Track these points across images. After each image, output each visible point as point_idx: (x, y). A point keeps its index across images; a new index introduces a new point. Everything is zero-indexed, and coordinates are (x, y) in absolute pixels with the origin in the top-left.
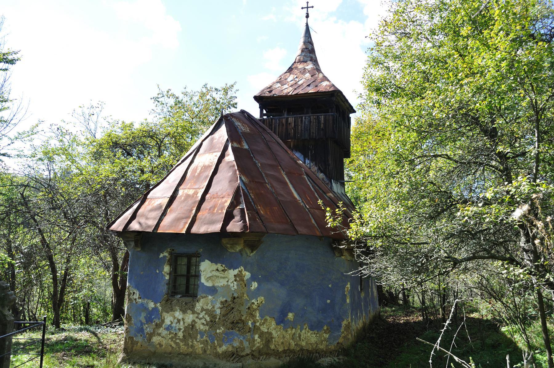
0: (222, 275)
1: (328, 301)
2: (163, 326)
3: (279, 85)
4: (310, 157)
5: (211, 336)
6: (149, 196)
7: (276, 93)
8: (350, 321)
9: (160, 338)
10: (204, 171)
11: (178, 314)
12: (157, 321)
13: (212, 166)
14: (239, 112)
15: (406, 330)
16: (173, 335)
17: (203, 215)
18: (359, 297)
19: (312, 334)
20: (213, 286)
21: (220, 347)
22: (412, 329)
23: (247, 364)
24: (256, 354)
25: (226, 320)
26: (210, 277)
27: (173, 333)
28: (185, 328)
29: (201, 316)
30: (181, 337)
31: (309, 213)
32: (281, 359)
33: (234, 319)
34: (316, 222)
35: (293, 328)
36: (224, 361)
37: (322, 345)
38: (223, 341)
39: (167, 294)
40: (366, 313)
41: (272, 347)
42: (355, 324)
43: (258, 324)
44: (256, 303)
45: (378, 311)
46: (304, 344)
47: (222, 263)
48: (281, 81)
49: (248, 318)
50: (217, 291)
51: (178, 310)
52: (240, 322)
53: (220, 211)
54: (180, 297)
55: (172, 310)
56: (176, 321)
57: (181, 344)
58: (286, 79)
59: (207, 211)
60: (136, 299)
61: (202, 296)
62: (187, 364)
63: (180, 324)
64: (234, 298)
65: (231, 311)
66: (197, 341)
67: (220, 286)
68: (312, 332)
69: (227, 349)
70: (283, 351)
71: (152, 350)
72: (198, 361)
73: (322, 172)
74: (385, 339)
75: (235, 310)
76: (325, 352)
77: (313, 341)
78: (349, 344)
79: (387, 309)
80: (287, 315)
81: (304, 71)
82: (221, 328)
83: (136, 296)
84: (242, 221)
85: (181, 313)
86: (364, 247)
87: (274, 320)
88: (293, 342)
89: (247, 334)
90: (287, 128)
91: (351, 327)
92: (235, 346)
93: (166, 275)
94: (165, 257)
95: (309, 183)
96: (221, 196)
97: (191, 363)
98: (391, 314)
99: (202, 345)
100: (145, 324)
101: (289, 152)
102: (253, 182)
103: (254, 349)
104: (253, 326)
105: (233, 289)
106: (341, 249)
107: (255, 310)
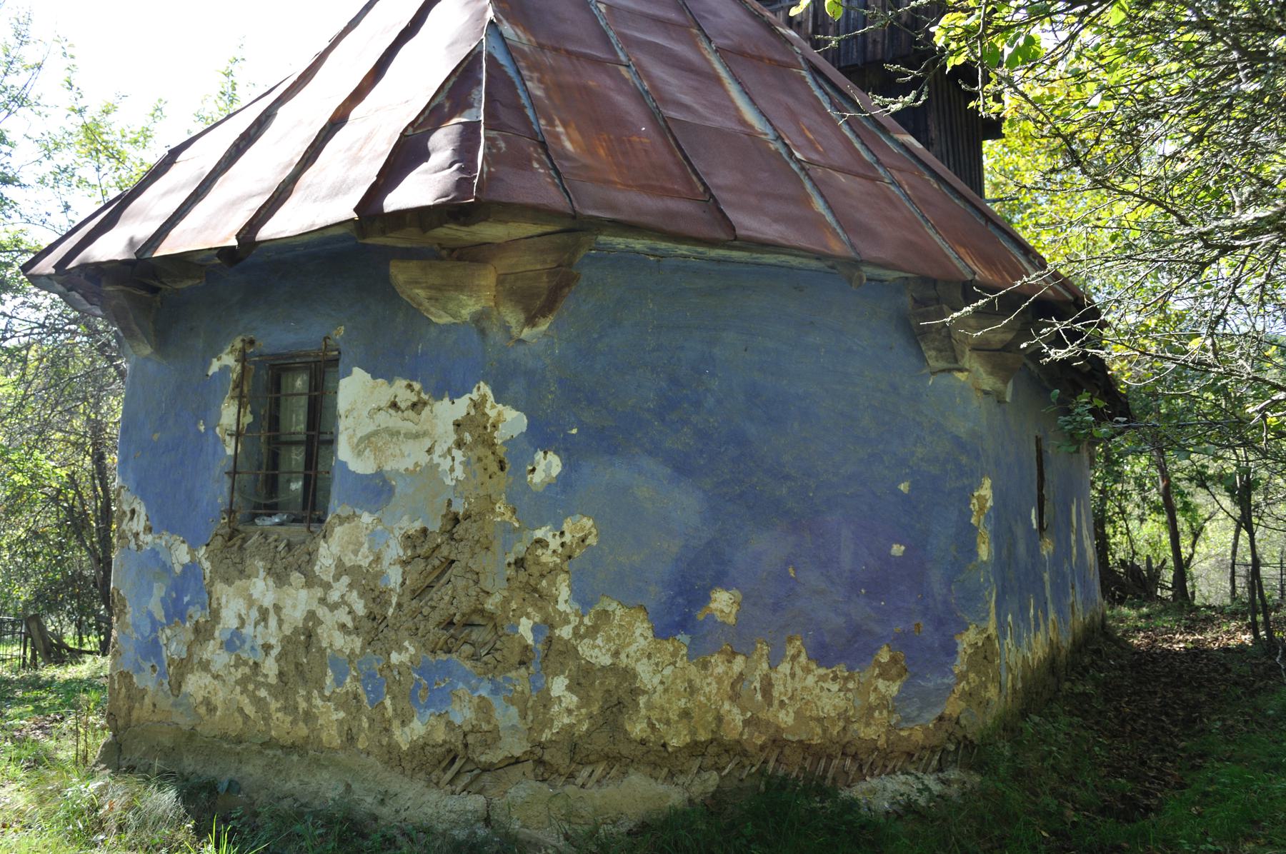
0: (409, 425)
1: (897, 550)
2: (217, 633)
8: (992, 630)
9: (207, 679)
11: (262, 588)
12: (199, 615)
15: (1201, 672)
16: (247, 670)
18: (1034, 552)
19: (822, 678)
20: (379, 474)
21: (403, 723)
22: (1221, 671)
24: (557, 758)
25: (426, 611)
26: (368, 437)
27: (245, 663)
28: (287, 640)
29: (334, 596)
30: (273, 680)
33: (452, 610)
34: (830, 207)
35: (734, 654)
36: (419, 785)
37: (868, 725)
38: (413, 696)
39: (231, 512)
40: (1059, 611)
42: (1018, 644)
44: (554, 543)
45: (1099, 611)
46: (786, 718)
50: (391, 490)
51: (262, 574)
52: (476, 619)
54: (281, 524)
55: (243, 574)
56: (254, 614)
57: (274, 705)
60: (136, 535)
61: (339, 516)
62: (289, 785)
63: (266, 627)
64: (456, 520)
65: (443, 573)
66: (323, 697)
67: (402, 470)
68: (822, 671)
69: (429, 733)
70: (687, 746)
71: (185, 722)
72: (325, 775)
74: (1128, 703)
75: (456, 569)
76: (886, 755)
78: (989, 721)
79: (1125, 610)
80: (707, 599)
82: (406, 644)
85: (270, 582)
87: (642, 615)
88: (736, 710)
89: (513, 674)
91: (999, 655)
93: (228, 438)
94: (225, 370)
97: (302, 783)
98: (1139, 624)
99: (342, 715)
103: (546, 736)
104: (542, 638)
105: (449, 482)
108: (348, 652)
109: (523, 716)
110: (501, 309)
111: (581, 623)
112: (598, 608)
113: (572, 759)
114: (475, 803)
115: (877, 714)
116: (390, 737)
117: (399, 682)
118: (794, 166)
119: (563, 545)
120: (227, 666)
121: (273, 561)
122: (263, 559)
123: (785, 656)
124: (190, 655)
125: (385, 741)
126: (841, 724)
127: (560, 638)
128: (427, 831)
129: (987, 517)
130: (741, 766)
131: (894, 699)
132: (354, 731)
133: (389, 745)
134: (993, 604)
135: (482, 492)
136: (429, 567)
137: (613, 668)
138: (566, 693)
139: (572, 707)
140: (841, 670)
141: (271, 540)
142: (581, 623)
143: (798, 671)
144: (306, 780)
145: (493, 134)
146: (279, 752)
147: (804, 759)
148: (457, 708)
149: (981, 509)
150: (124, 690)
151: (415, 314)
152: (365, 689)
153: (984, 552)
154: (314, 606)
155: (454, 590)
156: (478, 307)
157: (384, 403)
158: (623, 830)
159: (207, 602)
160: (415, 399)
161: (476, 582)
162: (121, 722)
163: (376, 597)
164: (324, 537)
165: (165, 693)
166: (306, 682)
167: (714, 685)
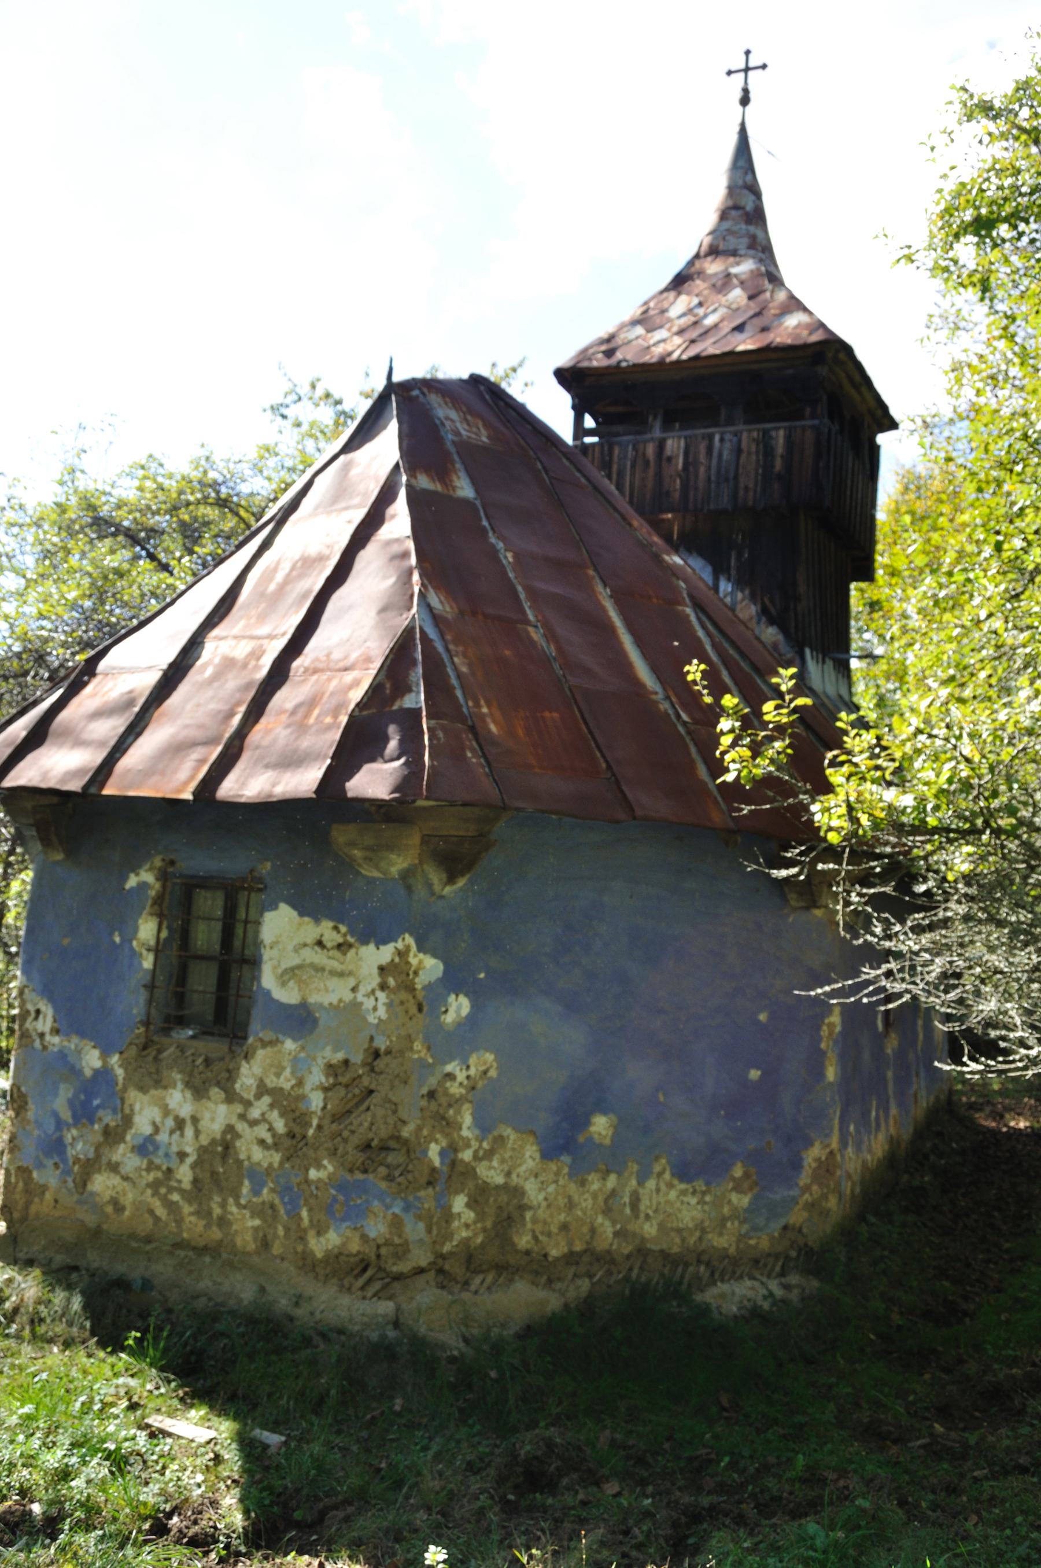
0: (335, 964)
1: (754, 1074)
2: (128, 1138)
3: (639, 330)
4: (733, 572)
5: (288, 1189)
6: (103, 665)
7: (626, 356)
8: (835, 1144)
9: (115, 1180)
10: (301, 576)
11: (179, 1100)
12: (109, 1119)
13: (328, 558)
14: (461, 381)
16: (159, 1175)
17: (268, 731)
19: (683, 1193)
20: (304, 1005)
21: (319, 1234)
23: (414, 1304)
25: (345, 1134)
26: (292, 969)
27: (158, 1168)
28: (202, 1151)
29: (255, 1113)
30: (186, 1185)
31: (688, 739)
32: (558, 1286)
33: (371, 1135)
35: (608, 1172)
36: (332, 1290)
37: (721, 1234)
38: (329, 1210)
39: (147, 1023)
40: (901, 1105)
41: (523, 1241)
43: (467, 1155)
44: (461, 1076)
46: (650, 1229)
47: (338, 917)
48: (646, 319)
49: (425, 1132)
50: (315, 1022)
51: (180, 1086)
52: (392, 1144)
53: (328, 720)
54: (193, 1037)
55: (160, 1083)
56: (170, 1123)
57: (187, 1209)
58: (663, 311)
59: (284, 718)
60: (42, 1035)
61: (261, 1040)
62: (202, 1285)
63: (182, 1135)
64: (377, 1054)
66: (238, 1205)
67: (326, 1003)
68: (683, 1186)
69: (344, 1244)
70: (565, 1256)
71: (91, 1220)
72: (239, 1277)
73: (771, 622)
75: (375, 1099)
76: (735, 1262)
77: (687, 1220)
78: (829, 1230)
80: (587, 1123)
81: (726, 281)
82: (325, 1162)
83: (45, 1024)
84: (402, 760)
85: (188, 1094)
86: (883, 878)
87: (532, 1139)
88: (607, 1223)
89: (422, 1194)
90: (659, 475)
92: (372, 1234)
93: (144, 952)
94: (143, 886)
95: (701, 633)
96: (341, 665)
97: (215, 1283)
99: (257, 1222)
100: (69, 1127)
101: (635, 523)
102: (474, 614)
103: (447, 1248)
104: (447, 1161)
105: (372, 1019)
106: (776, 881)
107: (456, 1102)
108: (265, 1165)
109: (429, 1231)
110: (425, 867)
111: (480, 1147)
112: (496, 1133)
113: (468, 1269)
114: (385, 1308)
115: (729, 1224)
116: (306, 1245)
117: (316, 1197)
118: (681, 729)
119: (468, 1077)
120: (138, 1169)
121: (191, 1075)
122: (180, 1072)
123: (651, 1173)
124: (98, 1156)
125: (300, 1248)
126: (698, 1234)
127: (462, 1161)
128: (341, 1332)
129: (836, 1042)
130: (609, 1273)
131: (746, 1210)
132: (269, 1237)
133: (304, 1252)
134: (836, 1121)
135: (403, 1032)
136: (350, 1095)
137: (505, 1187)
138: (466, 1210)
139: (469, 1221)
140: (700, 1185)
141: (189, 1053)
142: (480, 1147)
143: (663, 1187)
144: (219, 1280)
145: (433, 722)
146: (191, 1254)
147: (664, 1266)
148: (372, 1223)
149: (831, 1034)
150: (21, 1185)
151: (347, 866)
152: (282, 1199)
153: (831, 1073)
154: (234, 1120)
155: (374, 1116)
156: (405, 865)
157: (310, 940)
158: (511, 1332)
159: (119, 1107)
160: (341, 940)
161: (395, 1112)
162: (16, 1215)
163: (297, 1116)
164: (246, 1057)
165: (69, 1190)
166: (221, 1189)
167: (590, 1201)
